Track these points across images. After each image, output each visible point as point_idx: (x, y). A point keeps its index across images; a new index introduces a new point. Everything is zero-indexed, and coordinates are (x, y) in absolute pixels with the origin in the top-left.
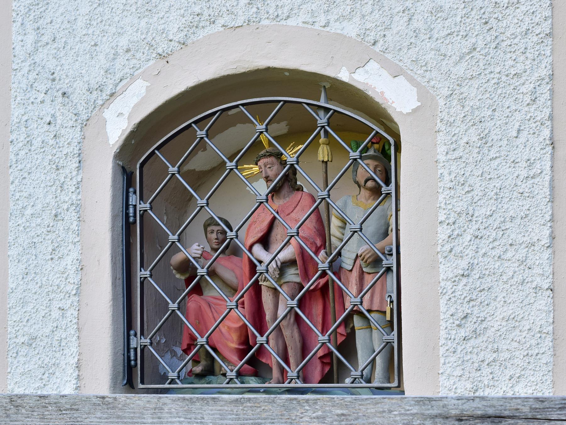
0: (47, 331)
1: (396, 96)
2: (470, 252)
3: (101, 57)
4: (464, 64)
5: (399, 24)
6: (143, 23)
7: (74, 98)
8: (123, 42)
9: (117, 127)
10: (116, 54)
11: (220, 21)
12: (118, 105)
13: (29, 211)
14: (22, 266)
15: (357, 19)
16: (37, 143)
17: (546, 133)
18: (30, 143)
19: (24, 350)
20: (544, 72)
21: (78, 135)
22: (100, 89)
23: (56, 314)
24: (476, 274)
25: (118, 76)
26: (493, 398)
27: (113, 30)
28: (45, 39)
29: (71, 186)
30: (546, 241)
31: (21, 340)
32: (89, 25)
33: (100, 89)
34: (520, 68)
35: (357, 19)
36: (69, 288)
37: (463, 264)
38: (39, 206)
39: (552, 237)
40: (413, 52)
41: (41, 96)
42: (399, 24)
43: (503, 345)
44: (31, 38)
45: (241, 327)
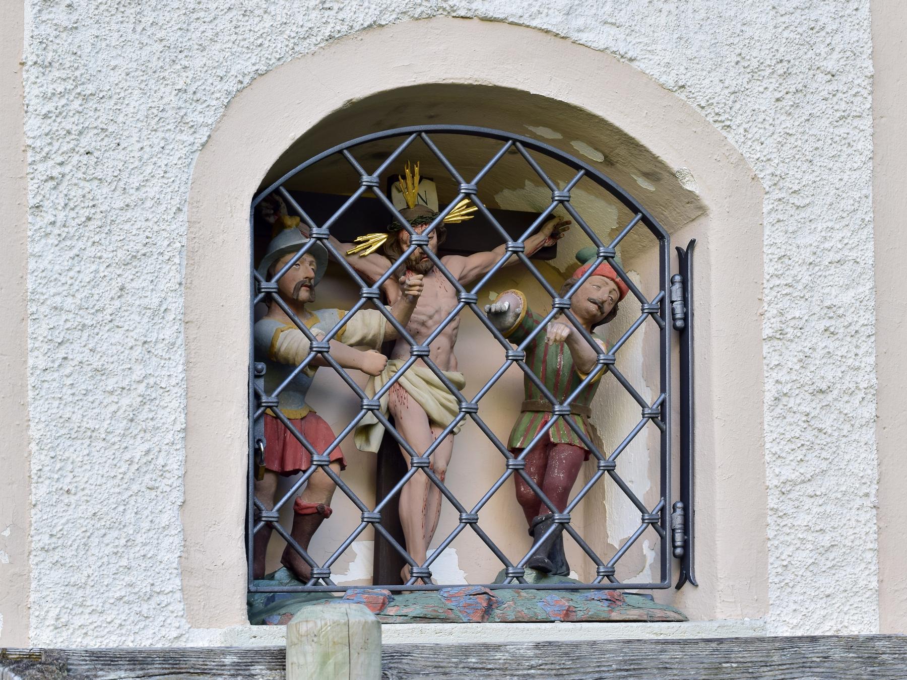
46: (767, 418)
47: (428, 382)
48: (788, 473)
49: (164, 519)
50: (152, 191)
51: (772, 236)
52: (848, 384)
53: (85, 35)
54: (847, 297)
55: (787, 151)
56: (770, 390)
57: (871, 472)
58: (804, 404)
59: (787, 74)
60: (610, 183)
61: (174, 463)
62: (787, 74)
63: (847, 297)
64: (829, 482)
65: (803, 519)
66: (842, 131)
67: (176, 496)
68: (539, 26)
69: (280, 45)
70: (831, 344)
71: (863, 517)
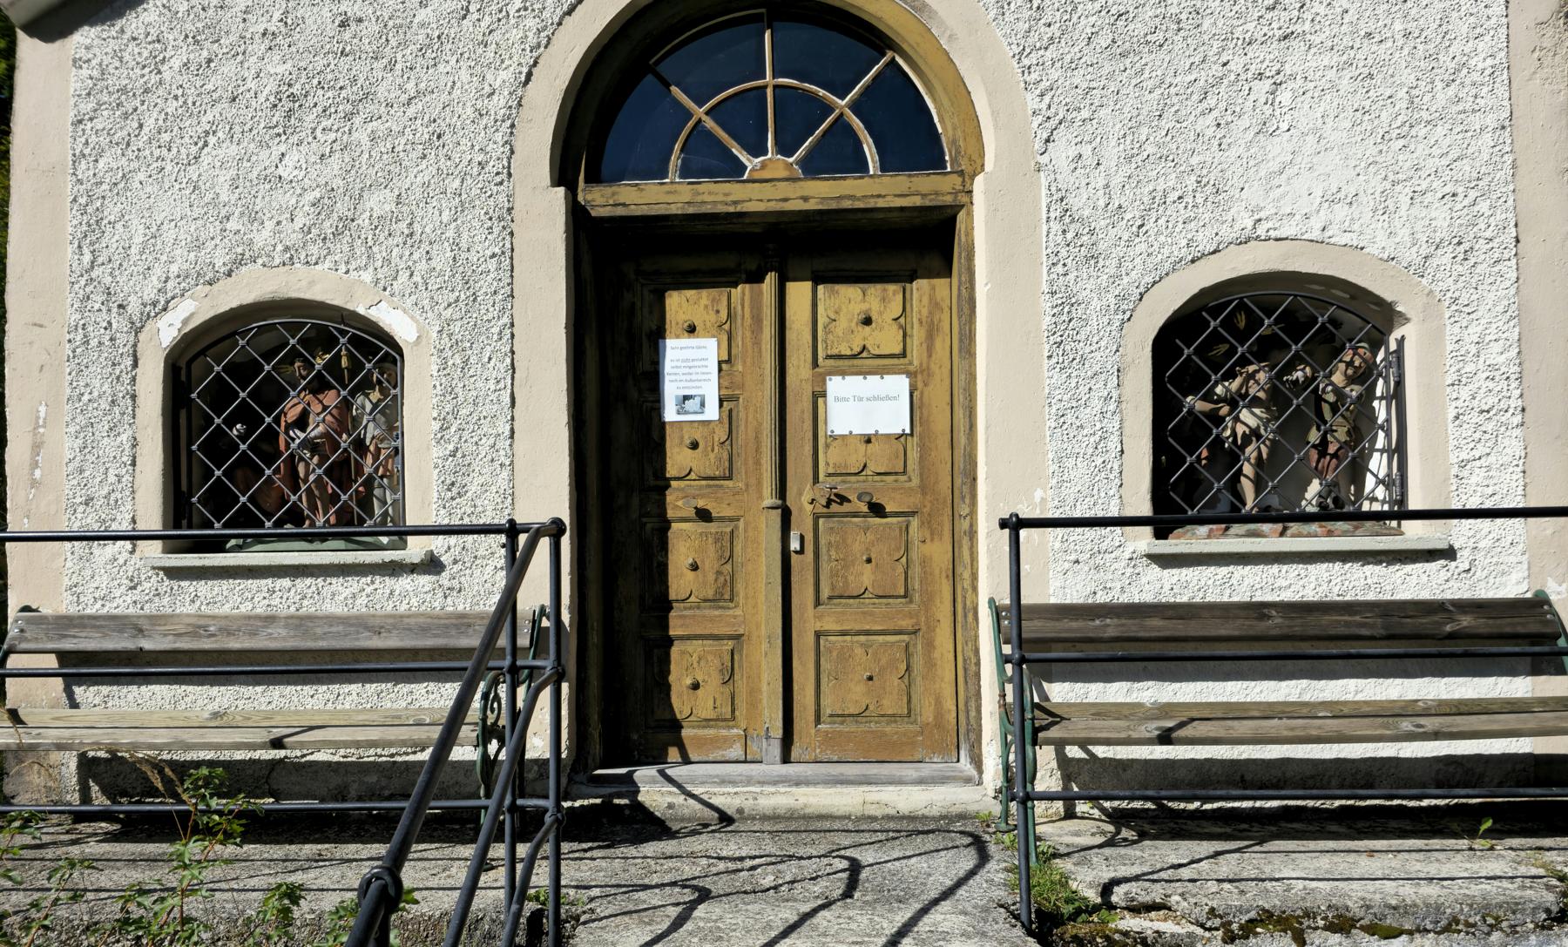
0: (104, 492)
1: (397, 322)
2: (456, 439)
3: (154, 279)
4: (450, 310)
5: (403, 277)
6: (192, 255)
7: (129, 309)
8: (174, 269)
9: (168, 330)
10: (167, 279)
11: (260, 261)
12: (168, 317)
13: (86, 398)
14: (80, 442)
15: (371, 269)
16: (94, 343)
17: (508, 361)
18: (87, 342)
19: (81, 509)
20: (505, 320)
21: (132, 338)
22: (154, 304)
23: (112, 479)
24: (459, 455)
25: (169, 295)
26: (182, 768)
27: (164, 258)
28: (100, 260)
29: (126, 379)
30: (507, 433)
31: (78, 500)
32: (142, 253)
33: (154, 304)
34: (490, 316)
35: (371, 269)
36: (125, 459)
37: (451, 447)
38: (96, 394)
39: (512, 431)
40: (413, 297)
41: (97, 306)
42: (403, 277)
43: (478, 502)
44: (87, 258)
45: (1451, 547)
46: (1451, 426)
47: (311, 728)
48: (1464, 456)
49: (1111, 493)
50: (1103, 343)
51: (1451, 331)
52: (1503, 405)
53: (1071, 277)
54: (1502, 359)
55: (1460, 285)
56: (1452, 413)
57: (1520, 452)
58: (1476, 418)
59: (1459, 243)
60: (794, 623)
61: (1116, 467)
62: (1459, 243)
63: (1502, 359)
64: (1492, 459)
65: (1474, 479)
66: (1496, 269)
67: (1117, 481)
68: (705, 797)
69: (1167, 266)
70: (1491, 385)
71: (1515, 477)
